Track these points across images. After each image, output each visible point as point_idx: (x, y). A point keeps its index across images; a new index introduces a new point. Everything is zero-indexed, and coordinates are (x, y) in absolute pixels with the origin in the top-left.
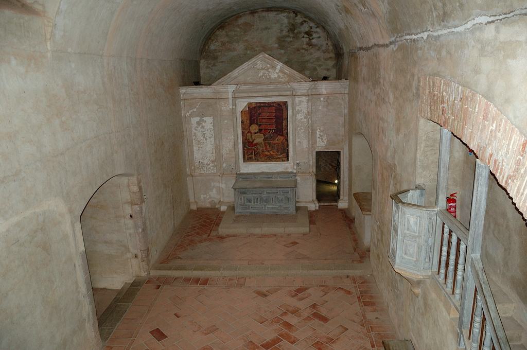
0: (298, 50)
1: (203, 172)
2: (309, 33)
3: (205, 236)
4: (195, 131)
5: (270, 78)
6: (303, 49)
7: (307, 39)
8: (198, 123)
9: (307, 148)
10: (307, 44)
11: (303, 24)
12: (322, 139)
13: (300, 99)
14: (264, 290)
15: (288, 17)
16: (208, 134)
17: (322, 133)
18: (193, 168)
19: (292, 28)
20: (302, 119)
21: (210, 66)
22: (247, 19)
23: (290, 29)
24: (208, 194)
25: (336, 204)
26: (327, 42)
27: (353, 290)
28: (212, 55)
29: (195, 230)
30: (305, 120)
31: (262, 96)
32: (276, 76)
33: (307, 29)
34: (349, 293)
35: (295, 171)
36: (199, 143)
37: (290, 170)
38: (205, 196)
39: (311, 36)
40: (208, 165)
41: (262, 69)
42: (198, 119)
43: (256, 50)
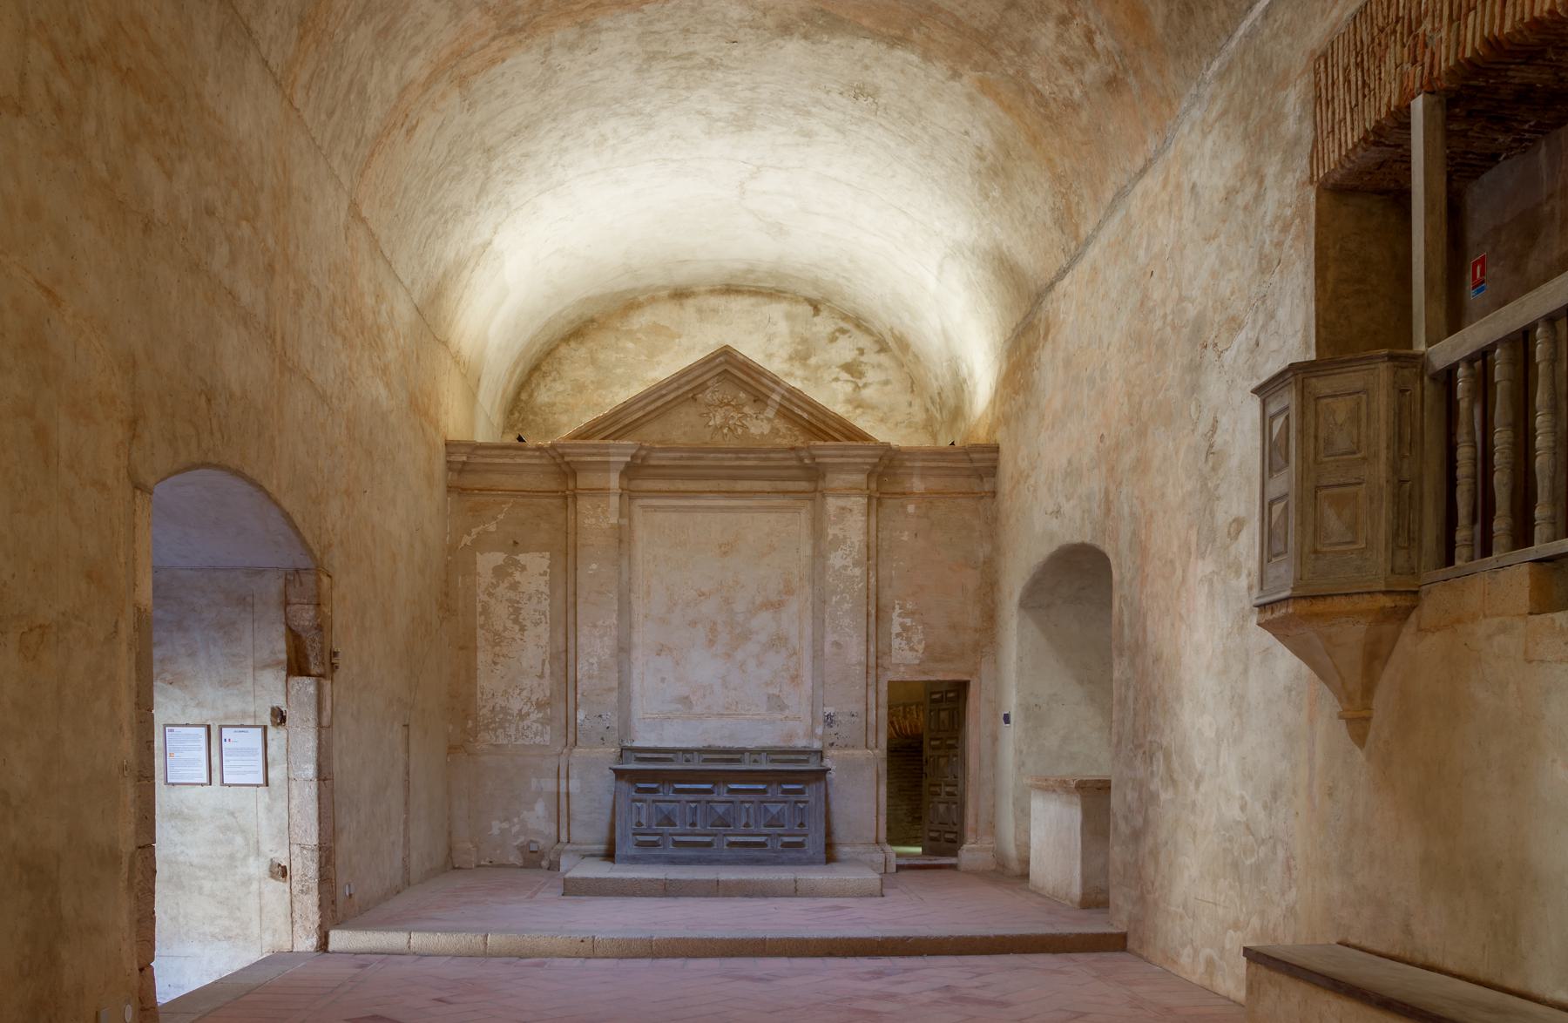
4: (485, 598)
7: (849, 388)
8: (500, 572)
9: (860, 663)
10: (849, 401)
12: (909, 640)
13: (841, 502)
15: (789, 317)
17: (908, 621)
18: (470, 724)
20: (845, 567)
22: (665, 314)
23: (797, 352)
25: (953, 861)
26: (908, 397)
28: (539, 420)
30: (857, 571)
32: (766, 428)
35: (817, 745)
36: (497, 639)
37: (801, 743)
38: (505, 825)
41: (722, 404)
42: (498, 558)
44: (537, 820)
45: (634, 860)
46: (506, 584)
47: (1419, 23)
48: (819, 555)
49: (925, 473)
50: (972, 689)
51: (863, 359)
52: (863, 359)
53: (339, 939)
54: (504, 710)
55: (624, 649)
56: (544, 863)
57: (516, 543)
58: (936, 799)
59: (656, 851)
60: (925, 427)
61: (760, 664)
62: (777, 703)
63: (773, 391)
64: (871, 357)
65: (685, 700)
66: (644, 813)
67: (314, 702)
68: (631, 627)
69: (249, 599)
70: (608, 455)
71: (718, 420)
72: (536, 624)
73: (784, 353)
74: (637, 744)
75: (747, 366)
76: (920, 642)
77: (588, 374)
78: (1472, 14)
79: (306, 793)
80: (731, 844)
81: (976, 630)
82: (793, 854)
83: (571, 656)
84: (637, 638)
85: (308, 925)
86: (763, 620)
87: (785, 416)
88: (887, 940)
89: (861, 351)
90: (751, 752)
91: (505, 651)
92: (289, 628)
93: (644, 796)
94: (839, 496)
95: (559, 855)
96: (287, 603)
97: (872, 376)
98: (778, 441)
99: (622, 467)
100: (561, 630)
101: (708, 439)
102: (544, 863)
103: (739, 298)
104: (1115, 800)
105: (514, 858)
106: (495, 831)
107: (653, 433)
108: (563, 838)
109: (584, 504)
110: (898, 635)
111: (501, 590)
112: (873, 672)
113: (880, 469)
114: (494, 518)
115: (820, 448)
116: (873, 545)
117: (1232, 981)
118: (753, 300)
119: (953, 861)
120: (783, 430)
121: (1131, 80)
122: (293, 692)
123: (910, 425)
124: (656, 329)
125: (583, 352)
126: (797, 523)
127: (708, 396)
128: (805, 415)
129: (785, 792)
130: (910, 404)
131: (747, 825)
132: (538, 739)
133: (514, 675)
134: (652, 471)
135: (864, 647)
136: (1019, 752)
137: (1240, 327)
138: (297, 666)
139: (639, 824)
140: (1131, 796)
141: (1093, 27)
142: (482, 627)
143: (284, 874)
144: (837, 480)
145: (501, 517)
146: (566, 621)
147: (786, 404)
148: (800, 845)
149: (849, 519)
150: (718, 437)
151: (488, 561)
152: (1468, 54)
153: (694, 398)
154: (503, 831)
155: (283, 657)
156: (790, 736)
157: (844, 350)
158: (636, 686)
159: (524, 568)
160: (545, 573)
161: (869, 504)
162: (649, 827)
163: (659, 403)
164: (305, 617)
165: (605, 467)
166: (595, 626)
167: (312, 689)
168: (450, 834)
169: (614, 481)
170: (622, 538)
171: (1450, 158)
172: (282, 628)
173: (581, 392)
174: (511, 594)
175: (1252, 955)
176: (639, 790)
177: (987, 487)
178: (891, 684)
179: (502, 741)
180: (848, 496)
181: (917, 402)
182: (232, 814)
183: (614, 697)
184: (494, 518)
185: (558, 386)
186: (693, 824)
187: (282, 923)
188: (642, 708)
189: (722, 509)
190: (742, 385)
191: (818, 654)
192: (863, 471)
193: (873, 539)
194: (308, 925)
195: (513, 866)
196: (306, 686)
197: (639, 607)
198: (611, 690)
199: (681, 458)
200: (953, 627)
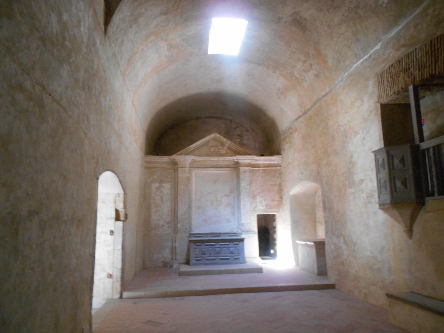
2: (240, 136)
7: (239, 140)
8: (158, 188)
20: (245, 186)
33: (239, 132)
40: (163, 226)
41: (214, 146)
42: (157, 185)
44: (167, 254)
45: (195, 264)
47: (409, 69)
53: (125, 294)
56: (169, 266)
57: (162, 181)
72: (167, 202)
74: (194, 232)
78: (426, 69)
80: (221, 259)
82: (237, 261)
83: (176, 209)
89: (242, 131)
93: (197, 247)
102: (169, 266)
104: (327, 248)
105: (160, 265)
108: (174, 258)
117: (383, 301)
121: (322, 75)
129: (235, 244)
137: (358, 134)
140: (333, 247)
141: (312, 63)
145: (158, 174)
152: (426, 77)
171: (409, 98)
175: (390, 296)
188: (195, 223)
195: (160, 267)
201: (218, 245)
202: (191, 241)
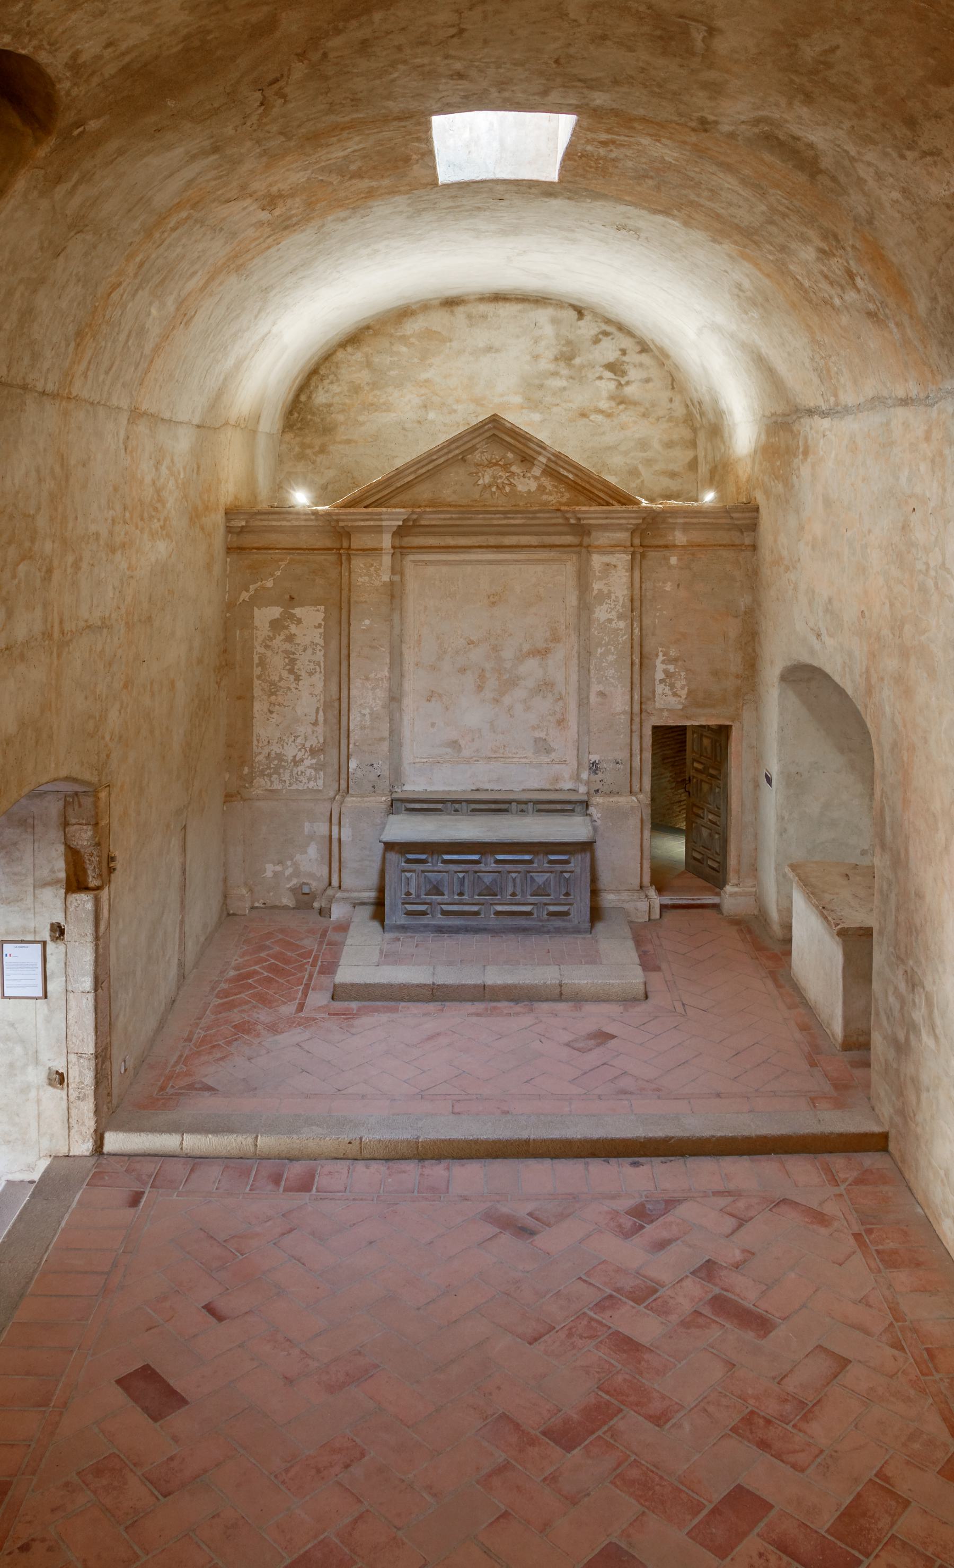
0: (583, 415)
1: (280, 787)
3: (288, 1009)
5: (514, 492)
6: (601, 412)
7: (612, 385)
8: (276, 625)
9: (624, 712)
10: (612, 398)
11: (600, 340)
14: (521, 1210)
15: (555, 321)
16: (304, 662)
17: (671, 668)
18: (246, 770)
19: (567, 356)
21: (308, 451)
22: (438, 320)
24: (289, 863)
26: (669, 394)
27: (830, 1208)
28: (317, 419)
29: (251, 986)
30: (622, 624)
31: (480, 547)
34: (820, 1218)
36: (273, 689)
38: (279, 868)
39: (622, 377)
40: (296, 762)
41: (491, 464)
42: (275, 612)
43: (455, 411)
46: (282, 637)
48: (584, 608)
49: (686, 528)
50: (734, 734)
51: (625, 359)
52: (625, 359)
53: (115, 1141)
54: (279, 757)
55: (395, 698)
57: (292, 598)
58: (699, 821)
59: (425, 921)
60: (685, 421)
61: (528, 709)
62: (543, 746)
63: (540, 454)
64: (633, 357)
65: (454, 745)
66: (413, 883)
67: (91, 917)
68: (402, 676)
69: (30, 821)
70: (381, 520)
71: (487, 479)
72: (311, 674)
73: (550, 354)
75: (515, 432)
76: (682, 688)
77: (364, 376)
79: (83, 1007)
80: (498, 913)
81: (737, 677)
82: (558, 923)
83: (344, 706)
84: (408, 686)
85: (84, 1130)
86: (532, 664)
87: (551, 475)
88: (650, 1141)
89: (624, 352)
90: (519, 802)
91: (280, 699)
92: (68, 847)
94: (604, 553)
95: (330, 902)
96: (66, 824)
97: (634, 374)
98: (545, 497)
99: (395, 529)
100: (335, 679)
101: (477, 497)
103: (507, 305)
106: (269, 874)
107: (424, 492)
108: (335, 883)
109: (358, 563)
110: (661, 681)
111: (278, 642)
112: (637, 719)
113: (644, 526)
114: (272, 575)
115: (585, 512)
116: (637, 597)
118: (519, 306)
119: (715, 900)
120: (549, 488)
122: (71, 909)
123: (670, 419)
124: (429, 334)
125: (359, 356)
126: (563, 573)
127: (477, 457)
128: (571, 476)
129: (551, 862)
130: (671, 400)
131: (514, 894)
132: (312, 784)
133: (290, 725)
134: (422, 530)
135: (629, 697)
136: (781, 818)
138: (76, 882)
139: (408, 894)
142: (259, 677)
143: (62, 1081)
144: (602, 538)
145: (278, 573)
146: (340, 670)
147: (552, 465)
148: (566, 914)
149: (613, 576)
150: (487, 495)
151: (265, 615)
153: (464, 460)
154: (276, 874)
155: (63, 875)
156: (557, 779)
157: (608, 351)
158: (406, 732)
159: (299, 621)
160: (319, 626)
161: (633, 559)
162: (418, 896)
163: (430, 466)
164: (83, 837)
165: (379, 530)
166: (367, 679)
167: (89, 906)
168: (225, 880)
169: (386, 541)
170: (394, 594)
172: (62, 848)
173: (357, 393)
174: (287, 646)
176: (408, 861)
177: (747, 541)
178: (655, 729)
179: (277, 786)
180: (612, 553)
181: (677, 399)
182: (12, 1025)
183: (385, 746)
184: (272, 575)
185: (335, 388)
186: (461, 894)
187: (59, 1128)
189: (490, 562)
190: (510, 447)
191: (583, 702)
192: (627, 530)
193: (637, 592)
194: (84, 1130)
195: (285, 908)
196: (84, 901)
197: (410, 657)
198: (382, 739)
199: (451, 519)
200: (715, 673)
201: (489, 864)
202: (389, 846)
